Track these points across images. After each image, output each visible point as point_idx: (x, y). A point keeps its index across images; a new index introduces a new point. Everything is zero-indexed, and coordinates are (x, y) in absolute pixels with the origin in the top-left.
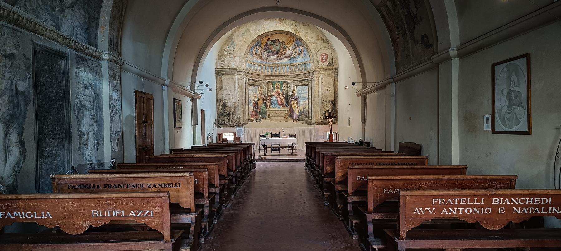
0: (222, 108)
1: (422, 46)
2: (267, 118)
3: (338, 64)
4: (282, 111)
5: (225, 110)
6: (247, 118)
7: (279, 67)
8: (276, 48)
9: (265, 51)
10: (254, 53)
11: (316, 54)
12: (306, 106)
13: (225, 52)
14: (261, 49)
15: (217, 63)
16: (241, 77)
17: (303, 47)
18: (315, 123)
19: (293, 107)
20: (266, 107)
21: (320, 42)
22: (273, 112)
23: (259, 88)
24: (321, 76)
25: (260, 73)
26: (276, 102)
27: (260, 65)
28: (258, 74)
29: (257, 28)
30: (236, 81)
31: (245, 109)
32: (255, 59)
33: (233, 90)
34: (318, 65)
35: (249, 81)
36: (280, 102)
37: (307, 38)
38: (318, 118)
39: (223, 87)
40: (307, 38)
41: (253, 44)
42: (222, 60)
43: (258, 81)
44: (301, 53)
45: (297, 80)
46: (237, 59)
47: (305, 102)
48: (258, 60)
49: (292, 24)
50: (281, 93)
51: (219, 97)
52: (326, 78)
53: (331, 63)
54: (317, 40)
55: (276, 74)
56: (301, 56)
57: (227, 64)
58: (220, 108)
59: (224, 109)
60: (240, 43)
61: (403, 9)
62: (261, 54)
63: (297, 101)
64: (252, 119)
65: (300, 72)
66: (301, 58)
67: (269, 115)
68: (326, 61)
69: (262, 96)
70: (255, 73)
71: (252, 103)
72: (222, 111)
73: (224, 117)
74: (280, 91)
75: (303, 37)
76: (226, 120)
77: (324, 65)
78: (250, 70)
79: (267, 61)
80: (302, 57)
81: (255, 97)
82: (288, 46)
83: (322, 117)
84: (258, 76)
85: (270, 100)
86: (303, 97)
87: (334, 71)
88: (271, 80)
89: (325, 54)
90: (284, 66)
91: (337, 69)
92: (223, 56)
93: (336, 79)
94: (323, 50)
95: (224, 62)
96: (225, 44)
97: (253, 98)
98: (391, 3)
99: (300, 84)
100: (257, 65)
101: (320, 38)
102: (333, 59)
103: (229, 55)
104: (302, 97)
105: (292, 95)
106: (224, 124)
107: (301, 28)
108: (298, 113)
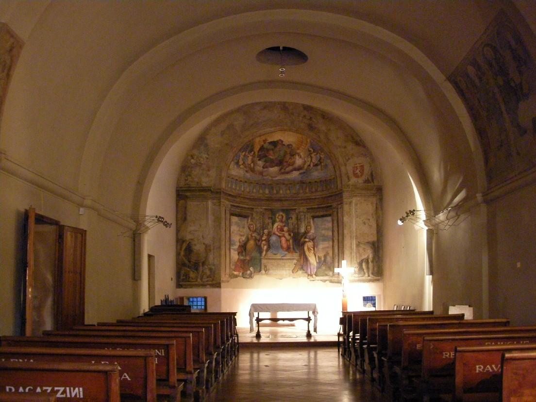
9: (259, 160)
10: (241, 162)
11: (346, 165)
12: (329, 252)
14: (254, 156)
19: (307, 253)
20: (261, 252)
21: (350, 146)
23: (249, 221)
24: (354, 200)
30: (210, 208)
35: (233, 209)
39: (188, 218)
42: (187, 173)
43: (248, 208)
45: (313, 207)
50: (286, 229)
53: (370, 179)
56: (319, 167)
57: (196, 180)
62: (252, 165)
64: (236, 273)
69: (253, 235)
73: (189, 269)
74: (284, 226)
77: (358, 182)
81: (241, 236)
82: (298, 151)
84: (247, 201)
85: (268, 241)
86: (323, 236)
87: (375, 192)
88: (269, 208)
89: (359, 164)
99: (318, 214)
100: (246, 182)
102: (373, 173)
106: (189, 281)
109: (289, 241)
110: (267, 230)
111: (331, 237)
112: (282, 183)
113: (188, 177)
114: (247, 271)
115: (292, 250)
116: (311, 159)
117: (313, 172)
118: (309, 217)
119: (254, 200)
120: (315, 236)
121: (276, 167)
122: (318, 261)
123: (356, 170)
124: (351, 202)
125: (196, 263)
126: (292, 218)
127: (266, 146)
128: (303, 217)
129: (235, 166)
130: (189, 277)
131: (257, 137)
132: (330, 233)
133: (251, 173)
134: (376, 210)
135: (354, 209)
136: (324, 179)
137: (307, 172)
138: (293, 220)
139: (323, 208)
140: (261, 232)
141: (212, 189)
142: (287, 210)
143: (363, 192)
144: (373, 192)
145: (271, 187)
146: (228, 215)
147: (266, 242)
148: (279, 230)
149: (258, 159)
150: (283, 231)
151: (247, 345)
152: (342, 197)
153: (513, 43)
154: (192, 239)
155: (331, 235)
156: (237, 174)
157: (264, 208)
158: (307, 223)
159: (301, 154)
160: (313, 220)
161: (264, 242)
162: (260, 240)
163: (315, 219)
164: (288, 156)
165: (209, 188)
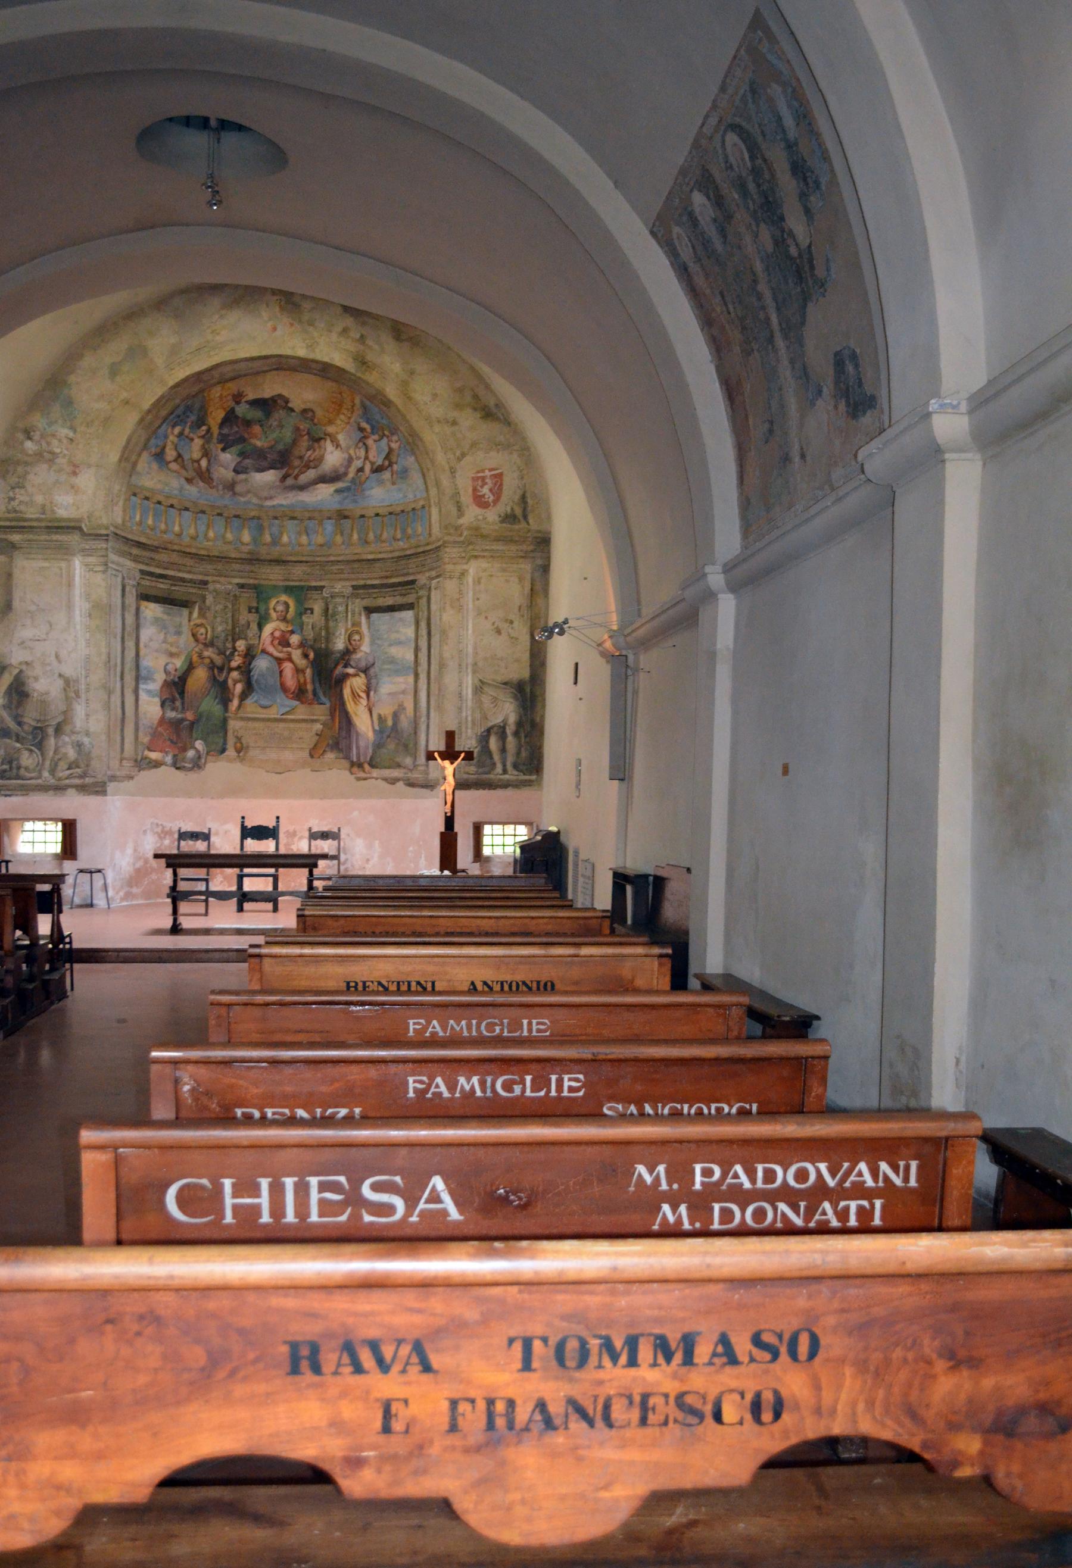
0: (10, 702)
1: (836, 407)
2: (231, 752)
4: (298, 725)
5: (20, 711)
7: (290, 525)
8: (274, 435)
9: (223, 450)
10: (170, 454)
11: (453, 471)
12: (405, 704)
13: (29, 444)
14: (207, 437)
16: (102, 560)
19: (350, 706)
20: (225, 702)
21: (468, 419)
22: (257, 725)
23: (195, 614)
24: (473, 569)
27: (203, 512)
28: (188, 550)
30: (77, 579)
31: (119, 711)
34: (461, 521)
35: (143, 582)
37: (410, 398)
39: (16, 604)
41: (164, 413)
42: (13, 480)
43: (191, 581)
44: (387, 463)
45: (369, 582)
46: (87, 480)
47: (403, 686)
49: (345, 331)
50: (295, 639)
53: (518, 512)
55: (276, 552)
56: (386, 475)
59: (17, 707)
60: (102, 405)
61: (758, 226)
62: (204, 463)
64: (154, 756)
65: (386, 547)
66: (388, 484)
67: (239, 739)
68: (496, 501)
69: (206, 654)
70: (176, 547)
73: (18, 745)
74: (292, 632)
75: (391, 392)
76: (27, 760)
78: (152, 529)
80: (394, 483)
81: (172, 655)
82: (331, 429)
84: (189, 562)
85: (246, 670)
86: (392, 661)
87: (531, 548)
88: (251, 581)
89: (491, 470)
91: (544, 542)
93: (538, 586)
95: (23, 491)
97: (163, 660)
98: (709, 198)
99: (382, 602)
100: (187, 509)
101: (468, 399)
102: (528, 495)
103: (47, 457)
106: (18, 777)
108: (371, 735)
109: (303, 671)
111: (412, 665)
112: (291, 515)
113: (17, 490)
114: (184, 749)
115: (310, 695)
116: (367, 452)
117: (372, 488)
118: (357, 610)
119: (209, 558)
120: (371, 661)
121: (272, 471)
122: (377, 728)
123: (482, 487)
124: (463, 574)
125: (40, 728)
126: (312, 611)
127: (241, 410)
128: (341, 609)
130: (19, 768)
131: (215, 385)
132: (410, 656)
133: (201, 484)
134: (532, 596)
135: (471, 594)
136: (398, 509)
137: (357, 487)
138: (315, 619)
139: (393, 585)
140: (229, 645)
141: (83, 526)
142: (301, 588)
144: (524, 547)
145: (257, 523)
146: (131, 599)
147: (242, 673)
148: (276, 642)
149: (221, 446)
152: (439, 559)
153: (789, 121)
154: (27, 663)
155: (412, 658)
156: (159, 486)
158: (353, 625)
159: (341, 437)
160: (368, 618)
161: (235, 674)
163: (374, 616)
164: (304, 442)
165: (77, 524)
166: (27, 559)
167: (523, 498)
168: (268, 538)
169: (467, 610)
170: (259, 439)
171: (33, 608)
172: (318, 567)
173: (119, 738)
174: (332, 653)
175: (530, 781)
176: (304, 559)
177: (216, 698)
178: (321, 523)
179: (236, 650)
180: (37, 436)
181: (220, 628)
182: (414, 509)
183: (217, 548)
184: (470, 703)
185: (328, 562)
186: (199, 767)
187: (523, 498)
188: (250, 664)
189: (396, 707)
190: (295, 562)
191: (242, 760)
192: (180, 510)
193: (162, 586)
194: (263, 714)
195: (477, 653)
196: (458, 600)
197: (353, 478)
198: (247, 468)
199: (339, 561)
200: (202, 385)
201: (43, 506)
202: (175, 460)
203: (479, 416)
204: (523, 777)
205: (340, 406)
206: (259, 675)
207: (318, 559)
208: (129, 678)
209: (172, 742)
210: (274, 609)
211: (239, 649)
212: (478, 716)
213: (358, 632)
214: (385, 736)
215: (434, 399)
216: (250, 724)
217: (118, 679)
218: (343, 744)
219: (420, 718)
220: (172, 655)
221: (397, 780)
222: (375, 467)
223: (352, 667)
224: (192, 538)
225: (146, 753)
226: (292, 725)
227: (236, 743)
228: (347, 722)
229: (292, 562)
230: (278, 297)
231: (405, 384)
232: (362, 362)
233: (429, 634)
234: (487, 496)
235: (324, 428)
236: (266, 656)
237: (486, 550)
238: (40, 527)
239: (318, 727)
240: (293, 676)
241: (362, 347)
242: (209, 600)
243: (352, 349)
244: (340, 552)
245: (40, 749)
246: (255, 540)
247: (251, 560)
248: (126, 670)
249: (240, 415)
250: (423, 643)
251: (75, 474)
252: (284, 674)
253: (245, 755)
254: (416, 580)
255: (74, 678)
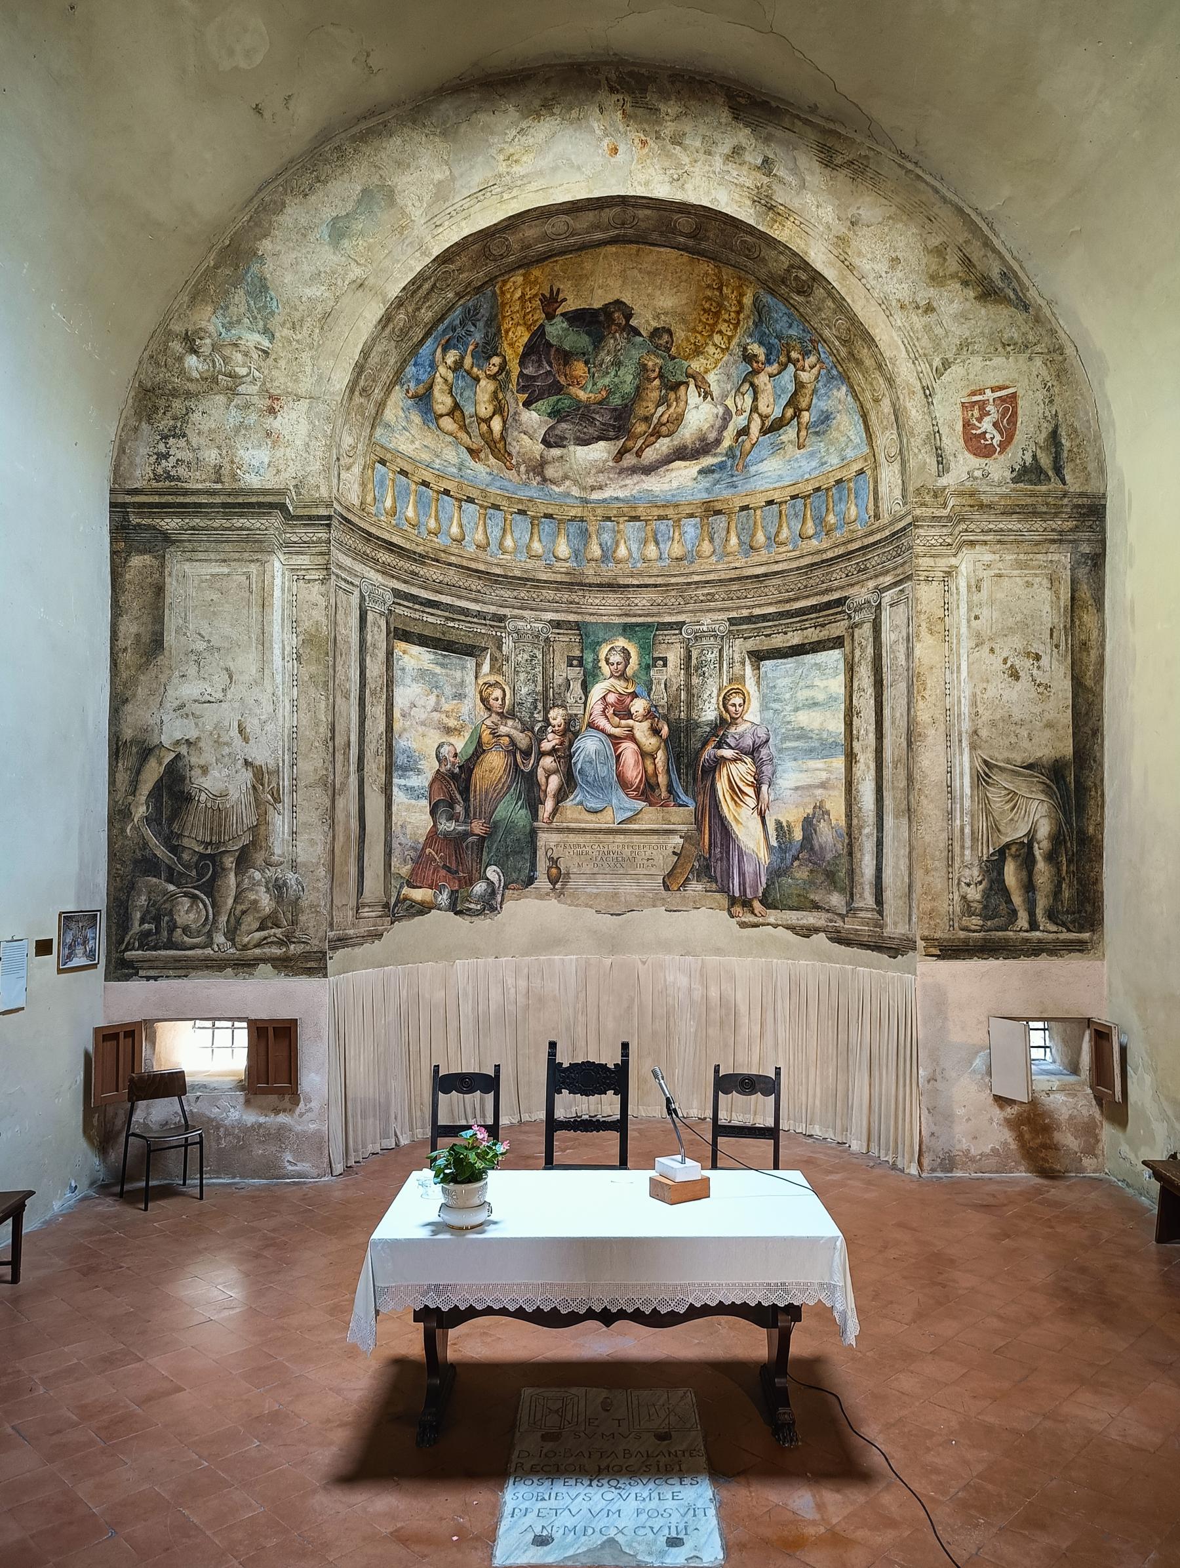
0: (158, 808)
2: (542, 883)
3: (1102, 470)
5: (176, 827)
6: (373, 886)
7: (630, 529)
8: (607, 381)
9: (527, 404)
10: (442, 401)
12: (828, 806)
13: (192, 361)
14: (500, 377)
15: (122, 450)
16: (321, 560)
17: (812, 359)
18: (921, 944)
19: (728, 808)
20: (533, 804)
23: (486, 668)
24: (967, 563)
25: (495, 561)
26: (603, 771)
27: (496, 507)
28: (473, 565)
29: (453, 179)
30: (277, 593)
31: (354, 824)
32: (452, 455)
33: (246, 663)
34: (943, 481)
35: (399, 610)
36: (632, 772)
37: (851, 268)
38: (943, 907)
39: (170, 639)
40: (856, 261)
41: (427, 315)
42: (165, 423)
43: (479, 614)
44: (790, 412)
45: (757, 611)
47: (824, 776)
48: (479, 467)
49: (737, 151)
51: (137, 716)
52: (1006, 582)
53: (1045, 461)
54: (933, 278)
55: (609, 571)
56: (789, 434)
57: (211, 456)
58: (140, 811)
59: (171, 820)
62: (497, 424)
63: (758, 764)
64: (418, 894)
67: (554, 861)
68: (1004, 446)
69: (503, 730)
70: (453, 559)
71: (419, 772)
72: (154, 841)
73: (171, 888)
74: (634, 695)
75: (819, 257)
76: (187, 914)
77: (985, 476)
79: (545, 480)
80: (800, 447)
81: (448, 731)
82: (696, 365)
83: (974, 894)
84: (475, 584)
85: (565, 754)
86: (802, 734)
87: (1070, 524)
88: (572, 618)
90: (665, 518)
92: (174, 393)
93: (1085, 592)
94: (977, 360)
95: (182, 443)
96: (193, 299)
97: (434, 738)
99: (778, 641)
100: (470, 500)
101: (953, 265)
102: (1063, 432)
103: (232, 386)
104: (798, 738)
105: (722, 720)
106: (171, 945)
107: (803, 186)
108: (763, 855)
110: (561, 711)
114: (470, 882)
116: (755, 399)
121: (602, 443)
122: (774, 843)
123: (980, 420)
125: (212, 857)
127: (556, 330)
129: (416, 419)
130: (173, 927)
131: (512, 270)
132: (837, 726)
133: (492, 460)
137: (737, 460)
138: (672, 672)
140: (539, 717)
142: (647, 626)
143: (1013, 524)
150: (629, 716)
151: (820, 278)
155: (841, 727)
157: (550, 616)
158: (731, 681)
159: (711, 378)
161: (547, 762)
162: (532, 751)
163: (767, 665)
166: (190, 560)
167: (1054, 435)
168: (596, 551)
169: (958, 635)
170: (583, 388)
171: (200, 646)
172: (673, 593)
173: (353, 870)
174: (698, 725)
175: (1082, 942)
176: (651, 581)
177: (519, 798)
178: (677, 523)
179: (550, 724)
180: (206, 345)
181: (524, 690)
182: (839, 482)
183: (519, 565)
184: (967, 803)
185: (689, 584)
186: (493, 909)
187: (1054, 435)
188: (571, 745)
189: (810, 811)
190: (638, 586)
191: (560, 895)
192: (460, 500)
193: (431, 619)
194: (592, 822)
195: (977, 714)
196: (942, 619)
197: (731, 448)
198: (563, 438)
199: (707, 582)
200: (491, 266)
201: (218, 469)
202: (451, 414)
203: (972, 294)
204: (1065, 936)
205: (717, 314)
206: (584, 762)
207: (673, 580)
208: (374, 768)
209: (449, 870)
210: (607, 660)
211: (553, 722)
212: (982, 824)
213: (739, 692)
214: (789, 856)
215: (892, 268)
216: (573, 838)
217: (353, 768)
218: (718, 869)
219: (861, 828)
220: (448, 731)
221: (817, 930)
222: (768, 423)
223: (731, 748)
224: (478, 546)
225: (406, 890)
226: (636, 839)
227: (549, 868)
228: (724, 833)
229: (633, 586)
230: (620, 97)
231: (842, 241)
232: (769, 207)
233: (879, 684)
234: (988, 436)
235: (686, 364)
236: (593, 732)
237: (990, 530)
238: (212, 505)
239: (677, 841)
240: (637, 762)
241: (766, 180)
242: (508, 645)
243: (749, 183)
244: (708, 568)
245: (210, 894)
246: (576, 554)
247: (572, 584)
248: (369, 755)
249: (554, 341)
250: (865, 703)
251: (272, 411)
252: (623, 759)
253: (564, 885)
254: (846, 598)
255: (271, 767)
